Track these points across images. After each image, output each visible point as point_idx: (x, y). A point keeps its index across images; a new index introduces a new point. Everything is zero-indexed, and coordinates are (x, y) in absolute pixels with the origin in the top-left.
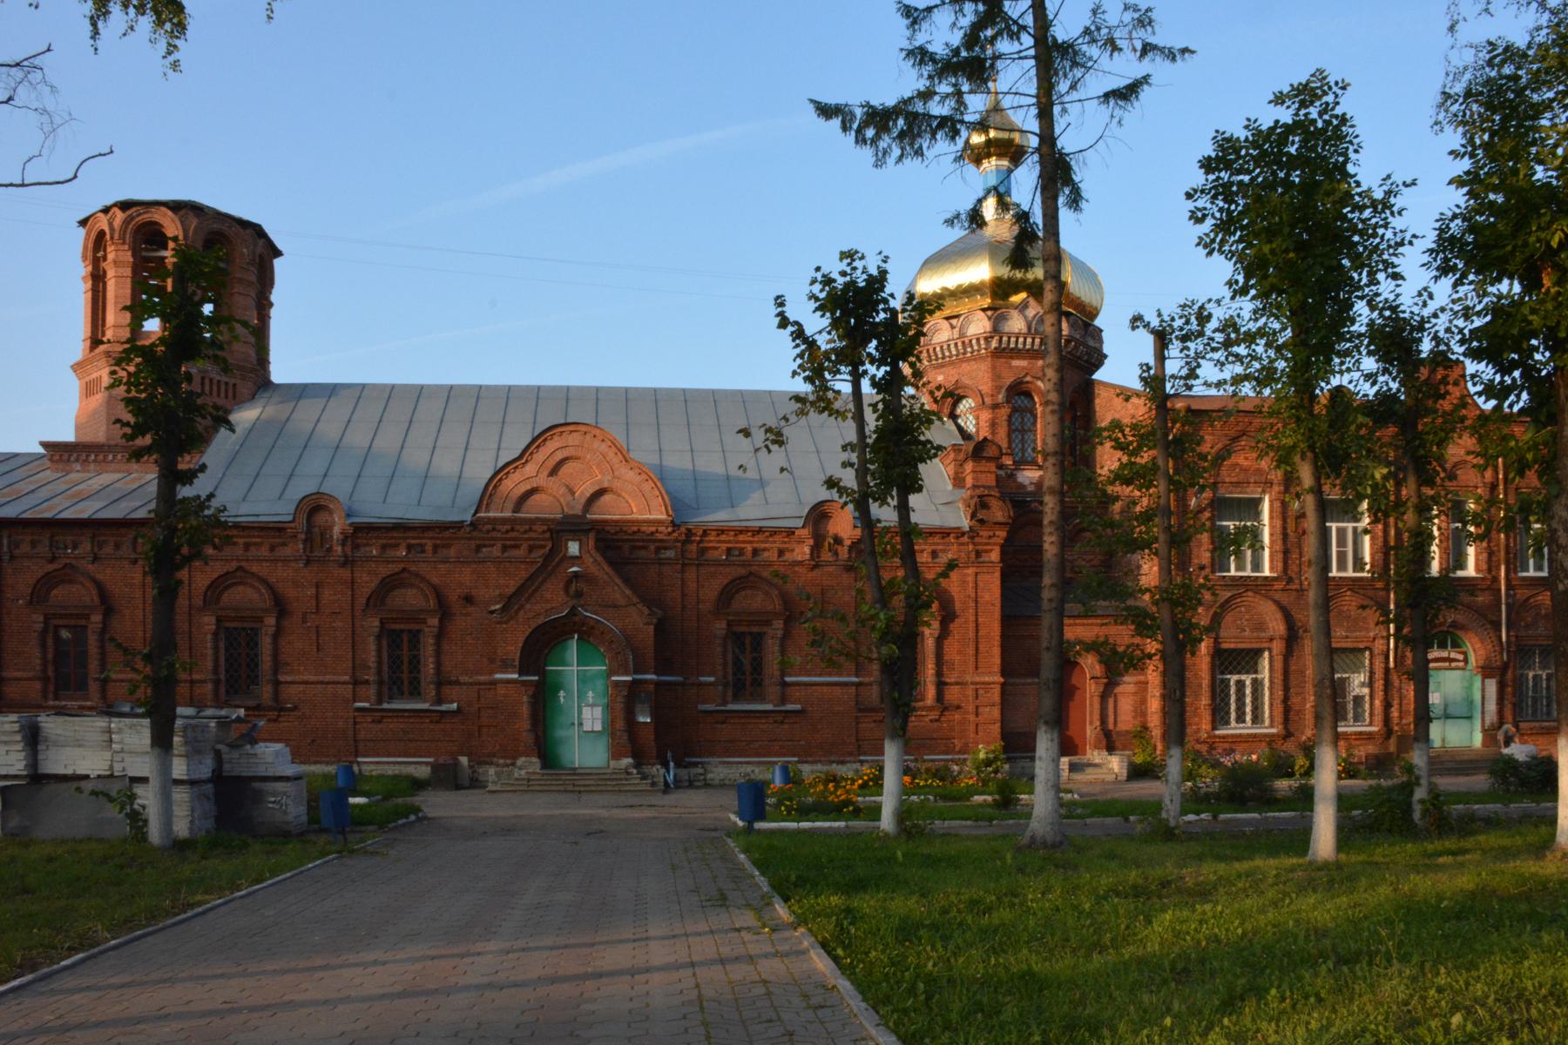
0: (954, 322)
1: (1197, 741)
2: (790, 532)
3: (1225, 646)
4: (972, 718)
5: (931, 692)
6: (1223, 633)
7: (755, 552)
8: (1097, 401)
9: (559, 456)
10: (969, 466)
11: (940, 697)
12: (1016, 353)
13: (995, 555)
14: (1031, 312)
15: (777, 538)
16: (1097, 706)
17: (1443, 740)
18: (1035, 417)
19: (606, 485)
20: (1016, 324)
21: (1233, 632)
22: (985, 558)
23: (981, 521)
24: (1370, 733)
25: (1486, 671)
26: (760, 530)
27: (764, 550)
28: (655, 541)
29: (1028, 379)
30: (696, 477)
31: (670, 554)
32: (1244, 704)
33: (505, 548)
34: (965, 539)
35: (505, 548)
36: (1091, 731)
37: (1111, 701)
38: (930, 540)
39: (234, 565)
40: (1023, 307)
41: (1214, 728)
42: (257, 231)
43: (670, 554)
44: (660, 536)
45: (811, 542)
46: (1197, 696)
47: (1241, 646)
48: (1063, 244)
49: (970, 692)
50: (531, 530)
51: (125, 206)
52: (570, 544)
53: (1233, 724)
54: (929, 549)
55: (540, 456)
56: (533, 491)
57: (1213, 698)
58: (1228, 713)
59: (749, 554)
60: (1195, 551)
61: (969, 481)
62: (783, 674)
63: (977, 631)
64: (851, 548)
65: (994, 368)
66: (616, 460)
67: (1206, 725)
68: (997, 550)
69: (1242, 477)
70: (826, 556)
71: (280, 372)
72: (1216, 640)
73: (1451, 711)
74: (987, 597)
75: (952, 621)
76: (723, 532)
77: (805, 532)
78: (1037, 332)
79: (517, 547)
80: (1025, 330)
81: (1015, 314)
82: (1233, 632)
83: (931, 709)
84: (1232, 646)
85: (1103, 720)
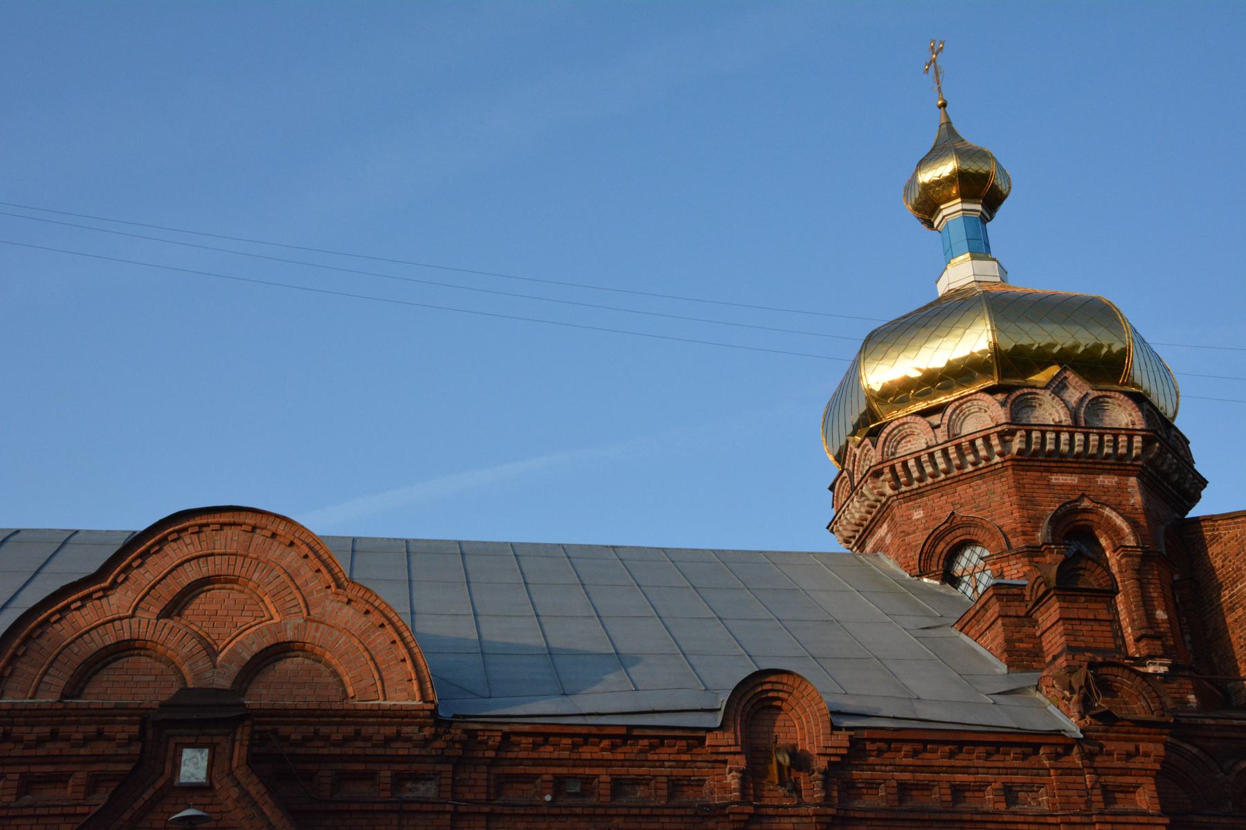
0: (936, 419)
2: (694, 738)
7: (618, 784)
8: (1213, 550)
9: (191, 574)
10: (1050, 614)
14: (1073, 395)
15: (664, 754)
19: (290, 635)
20: (1051, 411)
23: (1107, 718)
26: (628, 735)
27: (637, 781)
28: (392, 759)
29: (1086, 503)
30: (483, 650)
31: (427, 790)
33: (28, 784)
34: (1075, 759)
35: (28, 784)
38: (997, 761)
40: (1057, 386)
43: (427, 790)
44: (402, 749)
45: (741, 762)
50: (100, 735)
52: (187, 753)
54: (998, 781)
55: (145, 575)
56: (125, 648)
59: (605, 790)
61: (1054, 641)
64: (828, 776)
65: (1019, 487)
66: (315, 584)
70: (775, 795)
76: (546, 737)
77: (727, 739)
79: (59, 780)
80: (1069, 422)
81: (1046, 396)
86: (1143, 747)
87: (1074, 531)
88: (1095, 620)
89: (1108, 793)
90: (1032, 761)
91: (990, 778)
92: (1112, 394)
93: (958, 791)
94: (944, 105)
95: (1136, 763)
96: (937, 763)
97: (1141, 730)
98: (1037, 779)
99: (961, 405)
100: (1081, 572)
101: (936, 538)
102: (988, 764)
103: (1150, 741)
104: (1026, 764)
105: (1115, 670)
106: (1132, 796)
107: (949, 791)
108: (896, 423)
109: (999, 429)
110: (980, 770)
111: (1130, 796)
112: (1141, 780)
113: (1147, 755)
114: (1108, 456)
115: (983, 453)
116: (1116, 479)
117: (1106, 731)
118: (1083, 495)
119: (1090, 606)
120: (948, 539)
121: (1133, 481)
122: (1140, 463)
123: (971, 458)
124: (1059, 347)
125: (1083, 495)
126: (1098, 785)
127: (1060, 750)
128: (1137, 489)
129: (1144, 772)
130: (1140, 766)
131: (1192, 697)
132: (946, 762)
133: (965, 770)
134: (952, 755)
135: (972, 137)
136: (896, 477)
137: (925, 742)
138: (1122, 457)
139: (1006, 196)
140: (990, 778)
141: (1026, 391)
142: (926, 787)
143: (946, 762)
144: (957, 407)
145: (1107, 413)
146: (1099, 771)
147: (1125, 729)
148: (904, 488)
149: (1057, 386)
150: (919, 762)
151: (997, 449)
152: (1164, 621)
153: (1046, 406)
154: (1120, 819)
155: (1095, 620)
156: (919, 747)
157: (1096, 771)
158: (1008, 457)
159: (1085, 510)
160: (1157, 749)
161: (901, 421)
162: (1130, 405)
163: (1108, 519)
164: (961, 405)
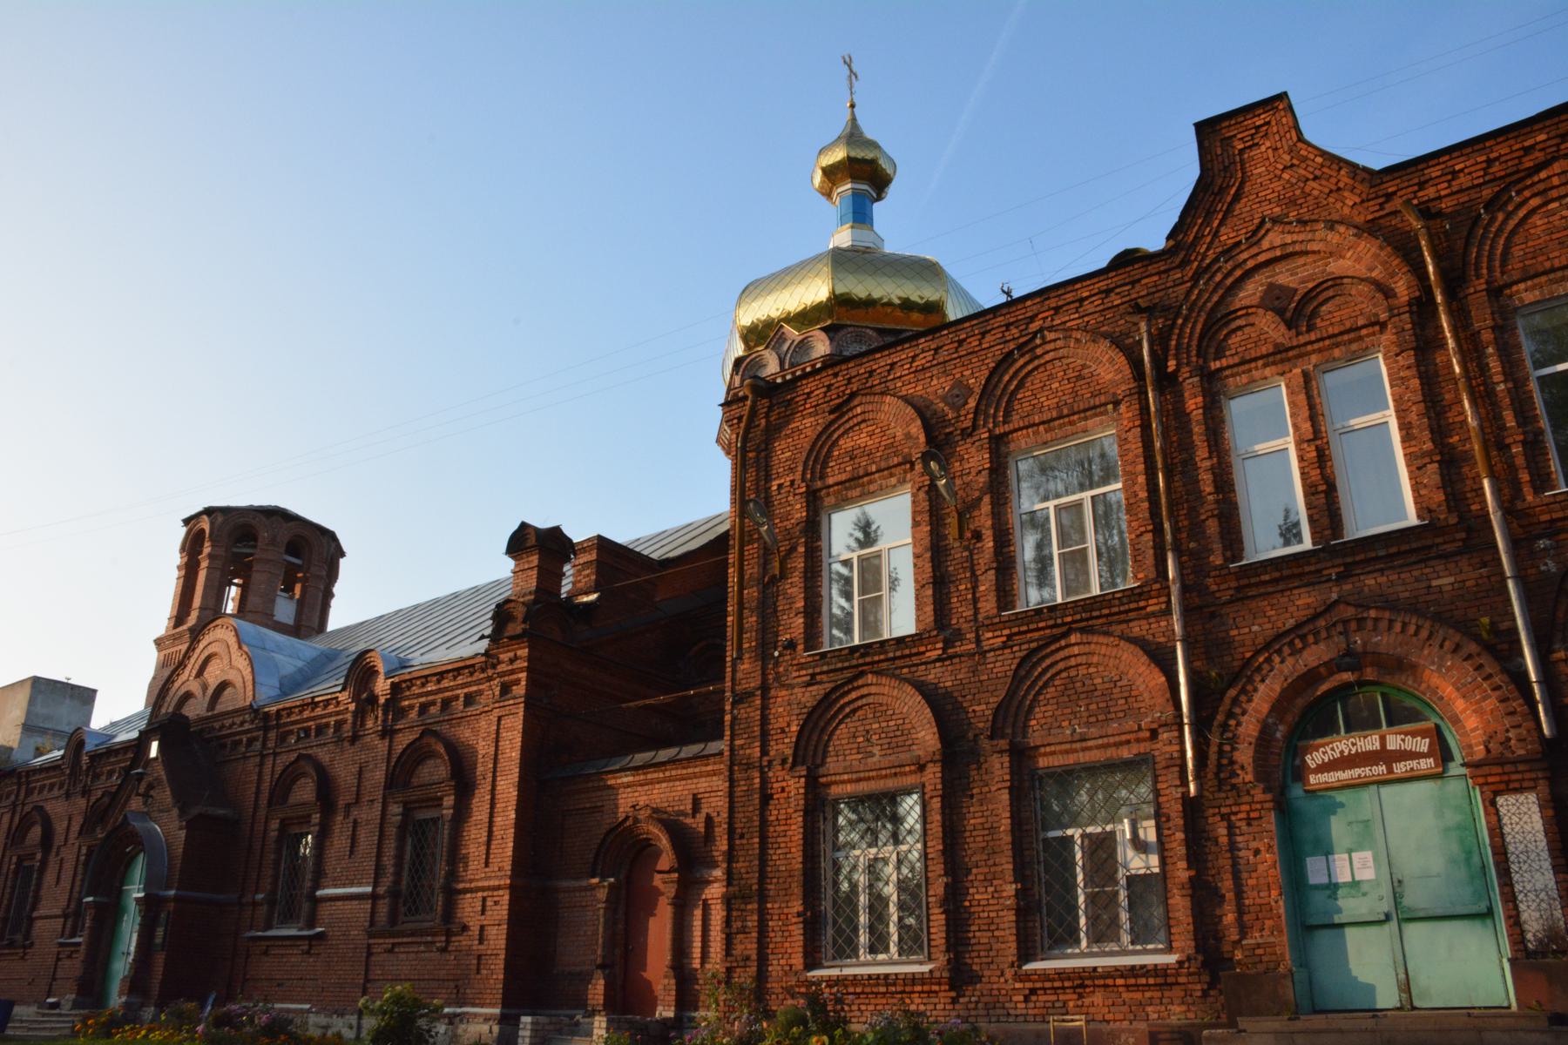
17: (1406, 987)
24: (1156, 971)
25: (1497, 774)
37: (698, 913)
39: (418, 730)
42: (330, 536)
51: (209, 511)
53: (864, 956)
62: (317, 886)
67: (798, 961)
71: (1500, 800)
73: (1415, 898)
86: (519, 653)
94: (853, 106)
129: (521, 670)
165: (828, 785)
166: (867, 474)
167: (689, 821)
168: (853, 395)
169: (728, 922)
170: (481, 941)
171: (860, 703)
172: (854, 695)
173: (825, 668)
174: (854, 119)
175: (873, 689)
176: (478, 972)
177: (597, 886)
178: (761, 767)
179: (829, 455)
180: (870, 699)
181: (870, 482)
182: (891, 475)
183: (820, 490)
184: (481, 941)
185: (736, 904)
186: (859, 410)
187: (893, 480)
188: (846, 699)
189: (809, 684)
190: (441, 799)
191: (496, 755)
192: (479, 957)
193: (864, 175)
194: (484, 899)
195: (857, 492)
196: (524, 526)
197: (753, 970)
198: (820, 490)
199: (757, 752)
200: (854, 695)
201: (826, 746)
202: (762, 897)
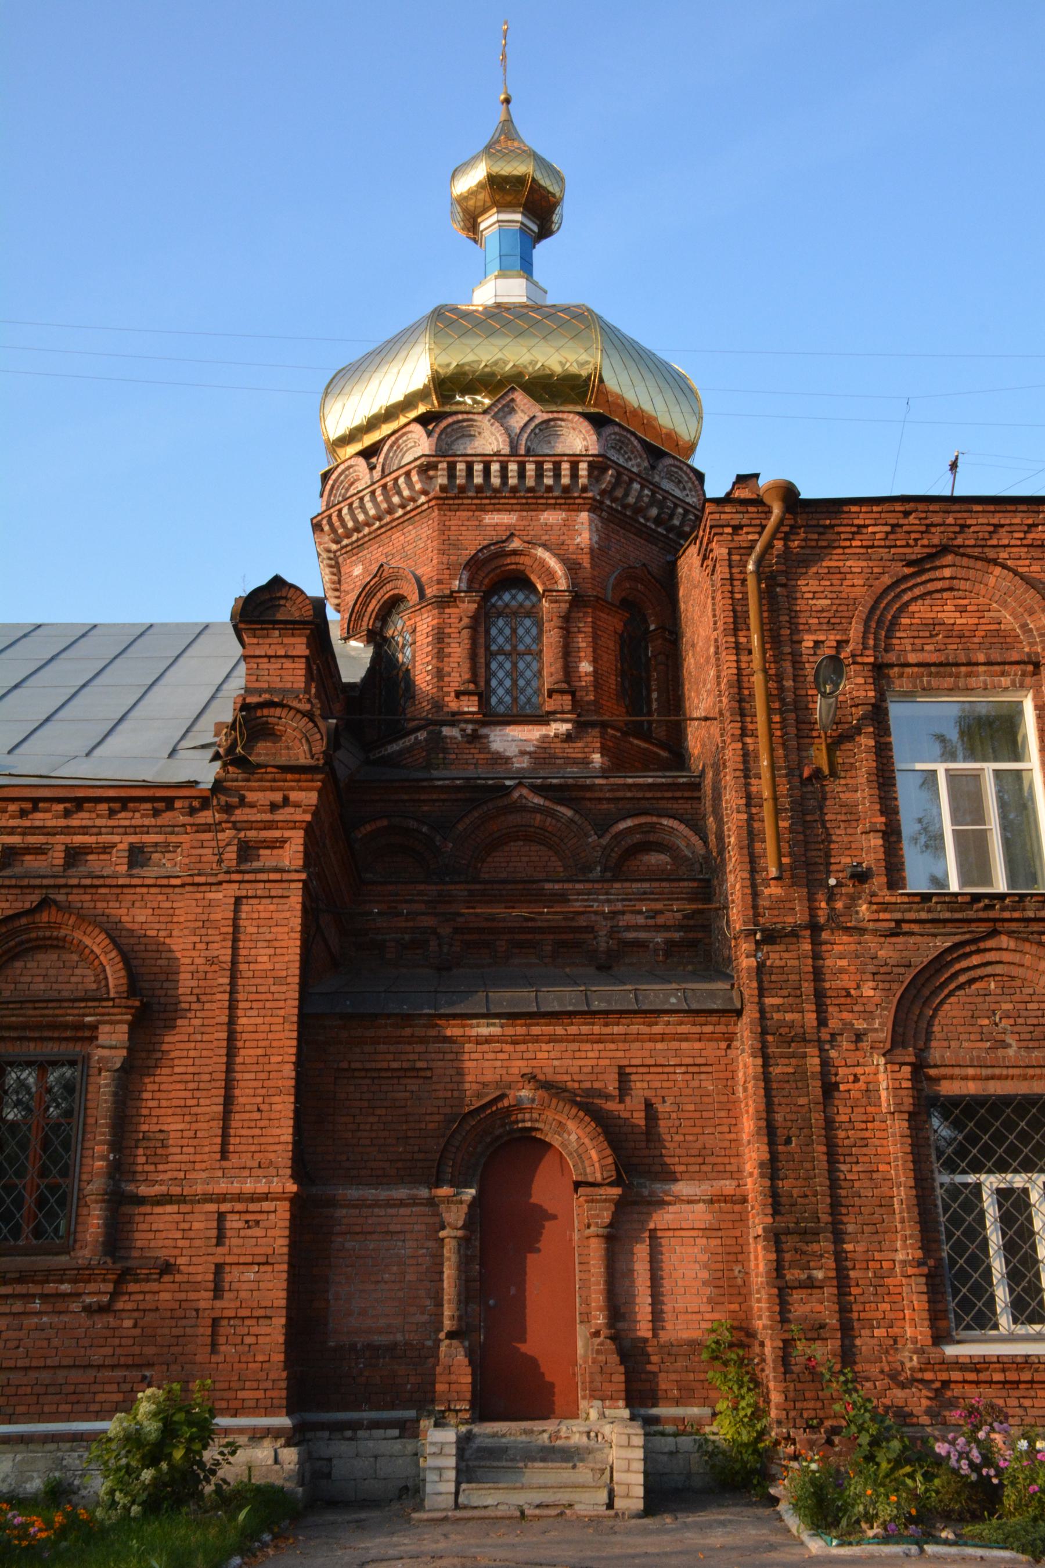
1: (894, 1377)
3: (948, 1089)
4: (204, 1299)
5: (93, 1222)
6: (937, 1053)
11: (117, 1238)
12: (488, 497)
13: (292, 854)
14: (517, 421)
16: (597, 1268)
18: (539, 624)
20: (490, 439)
21: (969, 1048)
22: (267, 858)
29: (516, 544)
32: (1009, 1248)
36: (587, 1345)
37: (642, 1250)
38: (123, 819)
40: (502, 412)
41: (940, 1338)
46: (879, 1232)
47: (996, 1088)
48: (534, 251)
49: (202, 1222)
57: (928, 1239)
58: (983, 1288)
60: (839, 835)
63: (231, 1052)
65: (443, 529)
67: (915, 1329)
68: (297, 838)
69: (954, 651)
72: (919, 1068)
74: (263, 958)
75: (170, 1025)
78: (528, 452)
80: (506, 450)
81: (484, 422)
82: (969, 1048)
83: (83, 1275)
84: (972, 1088)
85: (617, 1310)
86: (294, 796)
87: (496, 580)
88: (286, 656)
89: (247, 851)
90: (167, 818)
91: (116, 838)
92: (565, 416)
93: (74, 855)
94: (507, 101)
95: (284, 814)
96: (49, 823)
97: (289, 776)
98: (173, 839)
99: (397, 440)
100: (282, 602)
101: (367, 596)
102: (111, 823)
103: (301, 789)
104: (160, 821)
105: (278, 712)
106: (280, 851)
107: (62, 855)
108: (342, 467)
109: (418, 463)
110: (103, 830)
111: (276, 852)
112: (288, 834)
113: (297, 805)
114: (549, 489)
115: (406, 493)
116: (564, 515)
117: (248, 780)
118: (512, 535)
119: (286, 640)
120: (379, 595)
121: (584, 516)
122: (590, 495)
123: (396, 500)
124: (511, 365)
125: (512, 535)
126: (236, 841)
127: (196, 804)
128: (586, 526)
129: (293, 825)
130: (288, 818)
131: (597, 757)
132: (62, 822)
133: (84, 830)
134: (67, 813)
135: (531, 136)
136: (333, 529)
137: (35, 801)
138: (566, 489)
139: (562, 199)
140: (116, 838)
141: (460, 417)
142: (39, 851)
143: (62, 822)
144: (394, 443)
145: (562, 438)
146: (238, 825)
147: (269, 777)
148: (345, 542)
149: (502, 412)
150: (28, 823)
151: (418, 486)
152: (587, 674)
153: (486, 434)
154: (247, 877)
155: (286, 656)
156: (28, 806)
157: (236, 826)
158: (432, 495)
159: (515, 553)
160: (311, 798)
161: (346, 464)
162: (585, 426)
163: (543, 563)
164: (397, 440)
165: (937, 1080)
166: (969, 664)
167: (612, 1106)
168: (944, 549)
169: (778, 1269)
170: (218, 1291)
171: (979, 972)
172: (975, 960)
173: (923, 915)
174: (508, 121)
175: (1006, 957)
176: (214, 1346)
177: (448, 1200)
178: (819, 1040)
179: (894, 623)
180: (999, 969)
181: (969, 675)
182: (1003, 674)
183: (892, 666)
184: (218, 1291)
185: (790, 1242)
186: (947, 573)
187: (1005, 681)
188: (964, 964)
189: (894, 934)
190: (94, 1027)
191: (234, 963)
192: (215, 1322)
193: (534, 204)
194: (221, 1217)
195: (949, 682)
196: (277, 582)
197: (834, 1344)
198: (892, 666)
199: (811, 1018)
200: (975, 960)
201: (930, 1024)
202: (838, 1236)
